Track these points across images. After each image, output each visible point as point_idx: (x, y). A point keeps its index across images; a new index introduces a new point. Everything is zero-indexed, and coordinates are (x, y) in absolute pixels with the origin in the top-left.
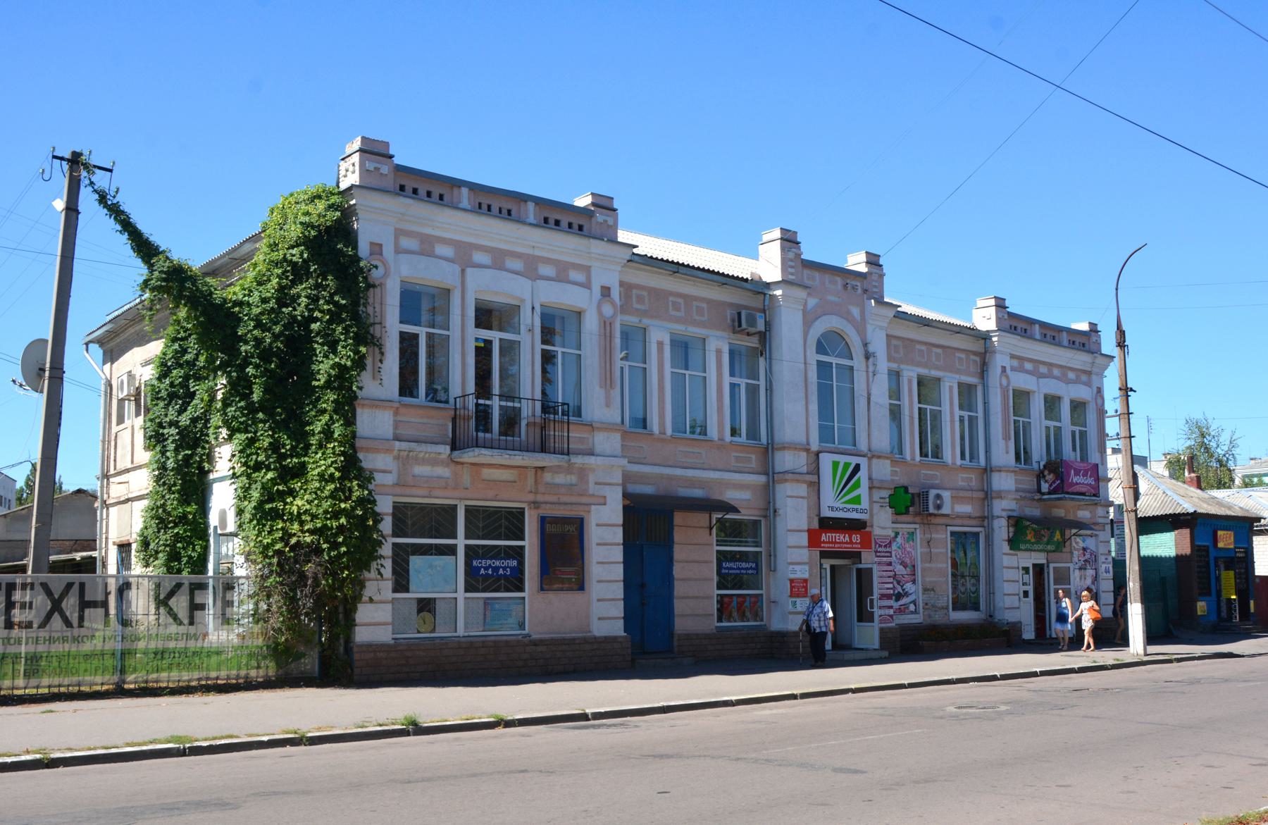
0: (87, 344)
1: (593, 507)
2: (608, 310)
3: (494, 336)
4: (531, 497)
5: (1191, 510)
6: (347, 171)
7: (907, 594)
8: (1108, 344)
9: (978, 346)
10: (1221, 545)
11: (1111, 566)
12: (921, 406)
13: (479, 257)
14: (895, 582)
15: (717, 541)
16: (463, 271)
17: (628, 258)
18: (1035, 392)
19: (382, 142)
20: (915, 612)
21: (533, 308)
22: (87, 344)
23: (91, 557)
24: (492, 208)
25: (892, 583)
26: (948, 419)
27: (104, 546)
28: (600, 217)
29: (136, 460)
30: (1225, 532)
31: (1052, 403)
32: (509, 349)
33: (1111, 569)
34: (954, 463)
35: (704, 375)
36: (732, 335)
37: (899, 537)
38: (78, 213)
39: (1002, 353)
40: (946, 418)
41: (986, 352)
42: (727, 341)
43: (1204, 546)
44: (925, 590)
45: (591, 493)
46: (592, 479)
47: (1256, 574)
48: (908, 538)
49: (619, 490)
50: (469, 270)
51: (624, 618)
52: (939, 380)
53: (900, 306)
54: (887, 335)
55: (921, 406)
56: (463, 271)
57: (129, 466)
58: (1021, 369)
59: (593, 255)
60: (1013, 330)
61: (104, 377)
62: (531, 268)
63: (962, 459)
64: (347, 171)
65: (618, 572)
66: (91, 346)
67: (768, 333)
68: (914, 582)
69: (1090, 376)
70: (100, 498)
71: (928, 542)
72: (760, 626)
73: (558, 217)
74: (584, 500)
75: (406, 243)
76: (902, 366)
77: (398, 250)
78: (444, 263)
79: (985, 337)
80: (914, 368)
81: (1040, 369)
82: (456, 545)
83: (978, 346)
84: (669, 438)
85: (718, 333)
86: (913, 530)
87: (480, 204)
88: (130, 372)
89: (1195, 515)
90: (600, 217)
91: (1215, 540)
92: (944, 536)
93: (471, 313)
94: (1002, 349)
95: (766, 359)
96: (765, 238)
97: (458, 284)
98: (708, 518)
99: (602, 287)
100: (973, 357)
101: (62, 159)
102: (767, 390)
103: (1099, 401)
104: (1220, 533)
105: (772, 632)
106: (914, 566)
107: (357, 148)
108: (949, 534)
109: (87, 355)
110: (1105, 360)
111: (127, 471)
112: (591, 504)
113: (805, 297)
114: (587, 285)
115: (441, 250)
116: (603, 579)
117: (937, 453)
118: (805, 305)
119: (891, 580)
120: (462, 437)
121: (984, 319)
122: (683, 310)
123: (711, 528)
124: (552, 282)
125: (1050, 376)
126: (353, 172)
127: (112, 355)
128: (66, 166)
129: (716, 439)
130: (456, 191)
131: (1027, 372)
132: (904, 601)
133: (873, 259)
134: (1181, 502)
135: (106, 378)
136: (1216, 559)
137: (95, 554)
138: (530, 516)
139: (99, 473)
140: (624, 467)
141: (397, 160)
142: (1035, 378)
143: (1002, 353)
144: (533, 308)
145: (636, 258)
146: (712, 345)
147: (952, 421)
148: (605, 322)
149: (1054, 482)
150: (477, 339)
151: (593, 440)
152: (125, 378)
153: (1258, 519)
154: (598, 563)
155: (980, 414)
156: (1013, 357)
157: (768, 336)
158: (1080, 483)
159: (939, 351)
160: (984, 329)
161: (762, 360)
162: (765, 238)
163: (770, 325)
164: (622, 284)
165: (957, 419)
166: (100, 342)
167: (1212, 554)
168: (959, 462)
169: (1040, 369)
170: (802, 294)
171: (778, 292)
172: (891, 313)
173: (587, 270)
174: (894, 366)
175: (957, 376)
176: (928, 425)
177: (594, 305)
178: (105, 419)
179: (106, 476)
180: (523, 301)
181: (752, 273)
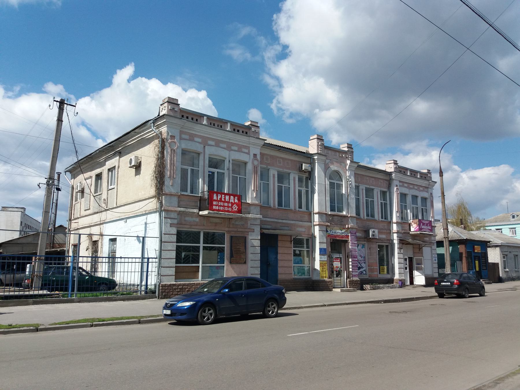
0: (65, 172)
1: (249, 233)
2: (256, 163)
3: (215, 171)
4: (227, 229)
5: (465, 238)
6: (162, 109)
7: (362, 268)
8: (435, 177)
9: (387, 178)
10: (476, 251)
11: (437, 258)
12: (366, 199)
13: (210, 142)
14: (358, 263)
15: (293, 246)
16: (204, 147)
17: (263, 144)
18: (408, 194)
19: (175, 99)
20: (366, 274)
21: (229, 161)
22: (65, 172)
23: (64, 250)
24: (215, 125)
25: (357, 263)
26: (377, 204)
27: (68, 246)
28: (253, 129)
29: (74, 217)
30: (478, 246)
31: (415, 197)
32: (221, 176)
33: (437, 260)
34: (379, 220)
35: (289, 186)
36: (299, 172)
37: (359, 246)
38: (62, 121)
39: (396, 180)
40: (376, 204)
41: (390, 180)
42: (297, 175)
43: (470, 251)
44: (369, 266)
45: (249, 228)
46: (249, 223)
47: (489, 262)
48: (362, 247)
49: (259, 227)
50: (206, 147)
51: (260, 274)
52: (373, 189)
53: (360, 163)
54: (355, 173)
55: (366, 199)
56: (204, 147)
57: (79, 216)
58: (403, 186)
59: (250, 143)
60: (400, 172)
61: (71, 184)
62: (229, 147)
63: (382, 218)
64: (162, 109)
65: (258, 257)
66: (67, 173)
67: (312, 172)
68: (365, 263)
69: (427, 188)
70: (68, 228)
71: (370, 248)
72: (310, 278)
73: (238, 129)
74: (247, 230)
75: (183, 136)
76: (360, 185)
77: (181, 139)
78: (198, 144)
79: (390, 174)
80: (364, 185)
81: (410, 186)
82: (200, 246)
83: (387, 178)
84: (277, 208)
85: (294, 172)
86: (364, 244)
87: (211, 123)
88: (81, 182)
89: (467, 240)
90: (253, 129)
91: (474, 249)
92: (375, 246)
93: (207, 162)
94: (396, 179)
95: (311, 181)
96: (311, 138)
97: (202, 151)
98: (290, 238)
99: (254, 154)
100: (386, 182)
101: (57, 101)
102: (311, 192)
103: (431, 198)
104: (475, 246)
105: (313, 280)
106: (365, 257)
107: (166, 101)
108: (377, 245)
109: (65, 176)
110: (433, 183)
111: (78, 218)
112: (249, 232)
113: (325, 159)
114: (248, 153)
115: (196, 139)
116: (253, 259)
117: (373, 216)
118: (325, 162)
119: (356, 262)
120: (203, 207)
121: (390, 168)
122: (282, 163)
123: (291, 241)
124: (236, 152)
125: (413, 188)
126: (165, 110)
127: (74, 177)
128: (58, 103)
129: (293, 209)
130: (202, 118)
131: (406, 187)
132: (361, 270)
133: (350, 146)
134: (461, 235)
135: (72, 184)
136: (475, 257)
137: (65, 249)
138: (227, 236)
139: (68, 219)
140: (260, 218)
141: (181, 106)
142: (408, 189)
143: (396, 180)
144: (229, 161)
145: (266, 144)
146: (292, 177)
147: (378, 205)
148: (255, 167)
149: (416, 227)
150: (209, 172)
151: (250, 209)
152: (79, 184)
153: (489, 242)
154: (251, 253)
155: (388, 202)
156: (400, 182)
157: (312, 173)
158: (424, 228)
159: (373, 179)
160: (58, 109)
161: (309, 181)
162: (311, 138)
163: (313, 169)
164: (261, 153)
165: (380, 204)
166: (70, 171)
167: (473, 254)
168: (380, 219)
169: (410, 186)
170: (324, 158)
171: (316, 157)
172: (356, 165)
173: (248, 148)
174: (357, 184)
175: (380, 188)
176: (370, 206)
177: (251, 161)
178: (71, 199)
179: (70, 220)
180: (226, 158)
181: (306, 150)
